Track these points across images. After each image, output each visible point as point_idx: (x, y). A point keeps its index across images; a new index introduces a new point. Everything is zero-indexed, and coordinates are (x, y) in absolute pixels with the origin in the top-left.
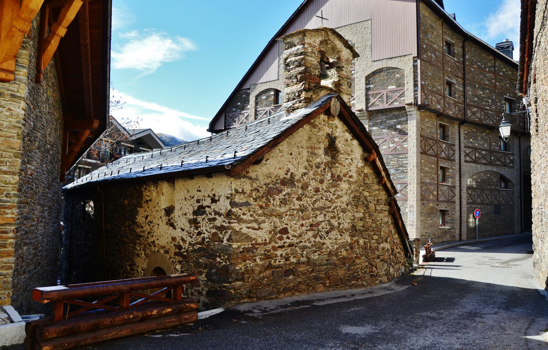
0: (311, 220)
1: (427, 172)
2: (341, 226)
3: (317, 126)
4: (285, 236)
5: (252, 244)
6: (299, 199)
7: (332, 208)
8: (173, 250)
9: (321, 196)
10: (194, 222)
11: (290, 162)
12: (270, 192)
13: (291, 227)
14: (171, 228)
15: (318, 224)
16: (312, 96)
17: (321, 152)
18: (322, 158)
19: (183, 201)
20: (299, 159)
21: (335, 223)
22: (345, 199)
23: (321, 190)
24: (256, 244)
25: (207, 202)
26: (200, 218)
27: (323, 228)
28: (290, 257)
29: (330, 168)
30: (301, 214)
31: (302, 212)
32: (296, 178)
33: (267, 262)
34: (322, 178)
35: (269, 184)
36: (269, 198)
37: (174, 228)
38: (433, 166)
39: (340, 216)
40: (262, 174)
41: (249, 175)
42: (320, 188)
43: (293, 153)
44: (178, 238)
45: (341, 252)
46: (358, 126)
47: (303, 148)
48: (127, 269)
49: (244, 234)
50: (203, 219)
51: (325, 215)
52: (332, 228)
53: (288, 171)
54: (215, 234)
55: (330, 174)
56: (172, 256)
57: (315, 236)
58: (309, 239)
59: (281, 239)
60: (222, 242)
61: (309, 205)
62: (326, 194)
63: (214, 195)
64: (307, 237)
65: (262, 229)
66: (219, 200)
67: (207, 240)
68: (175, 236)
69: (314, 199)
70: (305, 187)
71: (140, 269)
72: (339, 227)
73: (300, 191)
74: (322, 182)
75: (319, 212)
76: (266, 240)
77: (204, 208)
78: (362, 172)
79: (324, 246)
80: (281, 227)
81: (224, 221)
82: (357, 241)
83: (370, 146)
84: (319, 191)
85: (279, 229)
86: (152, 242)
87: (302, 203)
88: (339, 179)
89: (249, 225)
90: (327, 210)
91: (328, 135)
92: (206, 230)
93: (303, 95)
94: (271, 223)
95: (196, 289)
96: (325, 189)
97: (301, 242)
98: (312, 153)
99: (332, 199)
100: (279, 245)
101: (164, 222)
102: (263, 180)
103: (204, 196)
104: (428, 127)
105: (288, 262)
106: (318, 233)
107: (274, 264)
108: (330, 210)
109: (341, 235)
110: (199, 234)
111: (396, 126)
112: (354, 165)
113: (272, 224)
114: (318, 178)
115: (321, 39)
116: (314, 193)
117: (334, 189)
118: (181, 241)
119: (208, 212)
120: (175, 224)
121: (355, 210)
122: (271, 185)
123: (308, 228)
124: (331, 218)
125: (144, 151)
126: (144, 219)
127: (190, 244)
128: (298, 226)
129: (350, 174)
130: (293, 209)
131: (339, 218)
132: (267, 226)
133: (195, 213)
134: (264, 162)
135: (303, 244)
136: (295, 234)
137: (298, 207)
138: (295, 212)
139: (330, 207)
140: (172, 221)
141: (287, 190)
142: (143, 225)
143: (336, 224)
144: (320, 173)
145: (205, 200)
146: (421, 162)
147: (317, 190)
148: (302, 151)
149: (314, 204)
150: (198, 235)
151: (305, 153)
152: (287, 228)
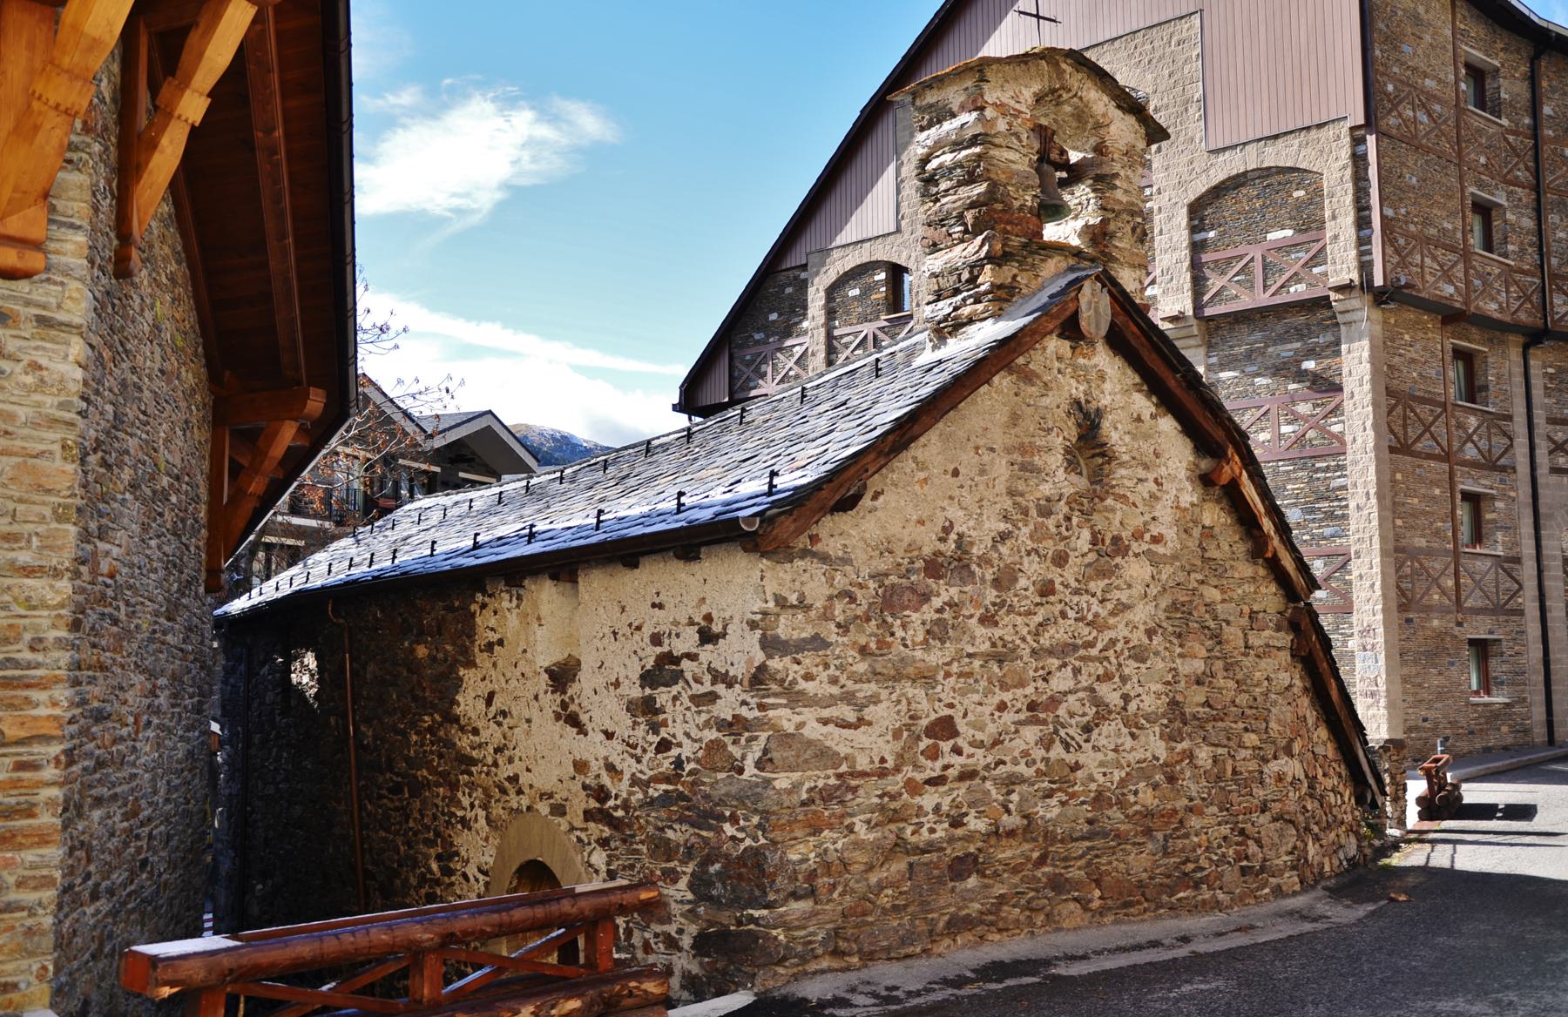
0: (1029, 690)
1: (1414, 514)
2: (1132, 707)
3: (1038, 377)
4: (946, 746)
5: (839, 776)
6: (988, 620)
7: (1100, 646)
8: (581, 803)
10: (646, 709)
11: (951, 498)
13: (965, 715)
15: (1054, 702)
16: (1015, 277)
17: (1056, 460)
18: (1059, 481)
19: (606, 640)
20: (981, 487)
22: (1142, 614)
23: (1058, 587)
25: (686, 641)
26: (663, 696)
27: (1072, 715)
30: (996, 668)
31: (1000, 662)
32: (975, 550)
34: (1061, 547)
35: (887, 575)
36: (890, 619)
38: (1437, 492)
40: (861, 544)
41: (819, 547)
42: (1058, 581)
47: (992, 450)
49: (810, 743)
50: (675, 698)
51: (1077, 671)
52: (1103, 712)
53: (947, 530)
55: (1086, 534)
56: (578, 823)
57: (1047, 743)
59: (933, 754)
61: (1024, 639)
62: (1076, 599)
64: (1018, 745)
65: (870, 724)
69: (1038, 619)
70: (1004, 580)
71: (471, 871)
72: (1124, 709)
73: (991, 595)
74: (1060, 560)
75: (1057, 663)
76: (883, 760)
77: (676, 660)
78: (1195, 522)
80: (933, 716)
81: (744, 703)
83: (1219, 434)
84: (1052, 592)
85: (924, 722)
87: (998, 632)
88: (1119, 547)
89: (826, 713)
90: (1082, 652)
93: (986, 278)
94: (899, 702)
95: (658, 928)
96: (1074, 584)
100: (928, 774)
102: (865, 564)
103: (676, 623)
104: (1413, 361)
105: (959, 832)
106: (1056, 732)
107: (913, 839)
108: (1094, 652)
109: (1133, 736)
112: (1167, 500)
113: (903, 706)
114: (1049, 547)
116: (1038, 600)
117: (1102, 584)
118: (604, 773)
119: (688, 675)
120: (584, 718)
122: (893, 579)
123: (1022, 716)
126: (481, 705)
127: (635, 781)
128: (987, 710)
129: (1155, 530)
130: (969, 655)
131: (1124, 679)
132: (884, 714)
136: (979, 736)
137: (986, 647)
138: (977, 663)
140: (572, 708)
141: (946, 592)
143: (1114, 699)
144: (1053, 530)
145: (678, 635)
146: (1394, 481)
147: (1046, 590)
148: (992, 462)
151: (1001, 468)
152: (951, 718)
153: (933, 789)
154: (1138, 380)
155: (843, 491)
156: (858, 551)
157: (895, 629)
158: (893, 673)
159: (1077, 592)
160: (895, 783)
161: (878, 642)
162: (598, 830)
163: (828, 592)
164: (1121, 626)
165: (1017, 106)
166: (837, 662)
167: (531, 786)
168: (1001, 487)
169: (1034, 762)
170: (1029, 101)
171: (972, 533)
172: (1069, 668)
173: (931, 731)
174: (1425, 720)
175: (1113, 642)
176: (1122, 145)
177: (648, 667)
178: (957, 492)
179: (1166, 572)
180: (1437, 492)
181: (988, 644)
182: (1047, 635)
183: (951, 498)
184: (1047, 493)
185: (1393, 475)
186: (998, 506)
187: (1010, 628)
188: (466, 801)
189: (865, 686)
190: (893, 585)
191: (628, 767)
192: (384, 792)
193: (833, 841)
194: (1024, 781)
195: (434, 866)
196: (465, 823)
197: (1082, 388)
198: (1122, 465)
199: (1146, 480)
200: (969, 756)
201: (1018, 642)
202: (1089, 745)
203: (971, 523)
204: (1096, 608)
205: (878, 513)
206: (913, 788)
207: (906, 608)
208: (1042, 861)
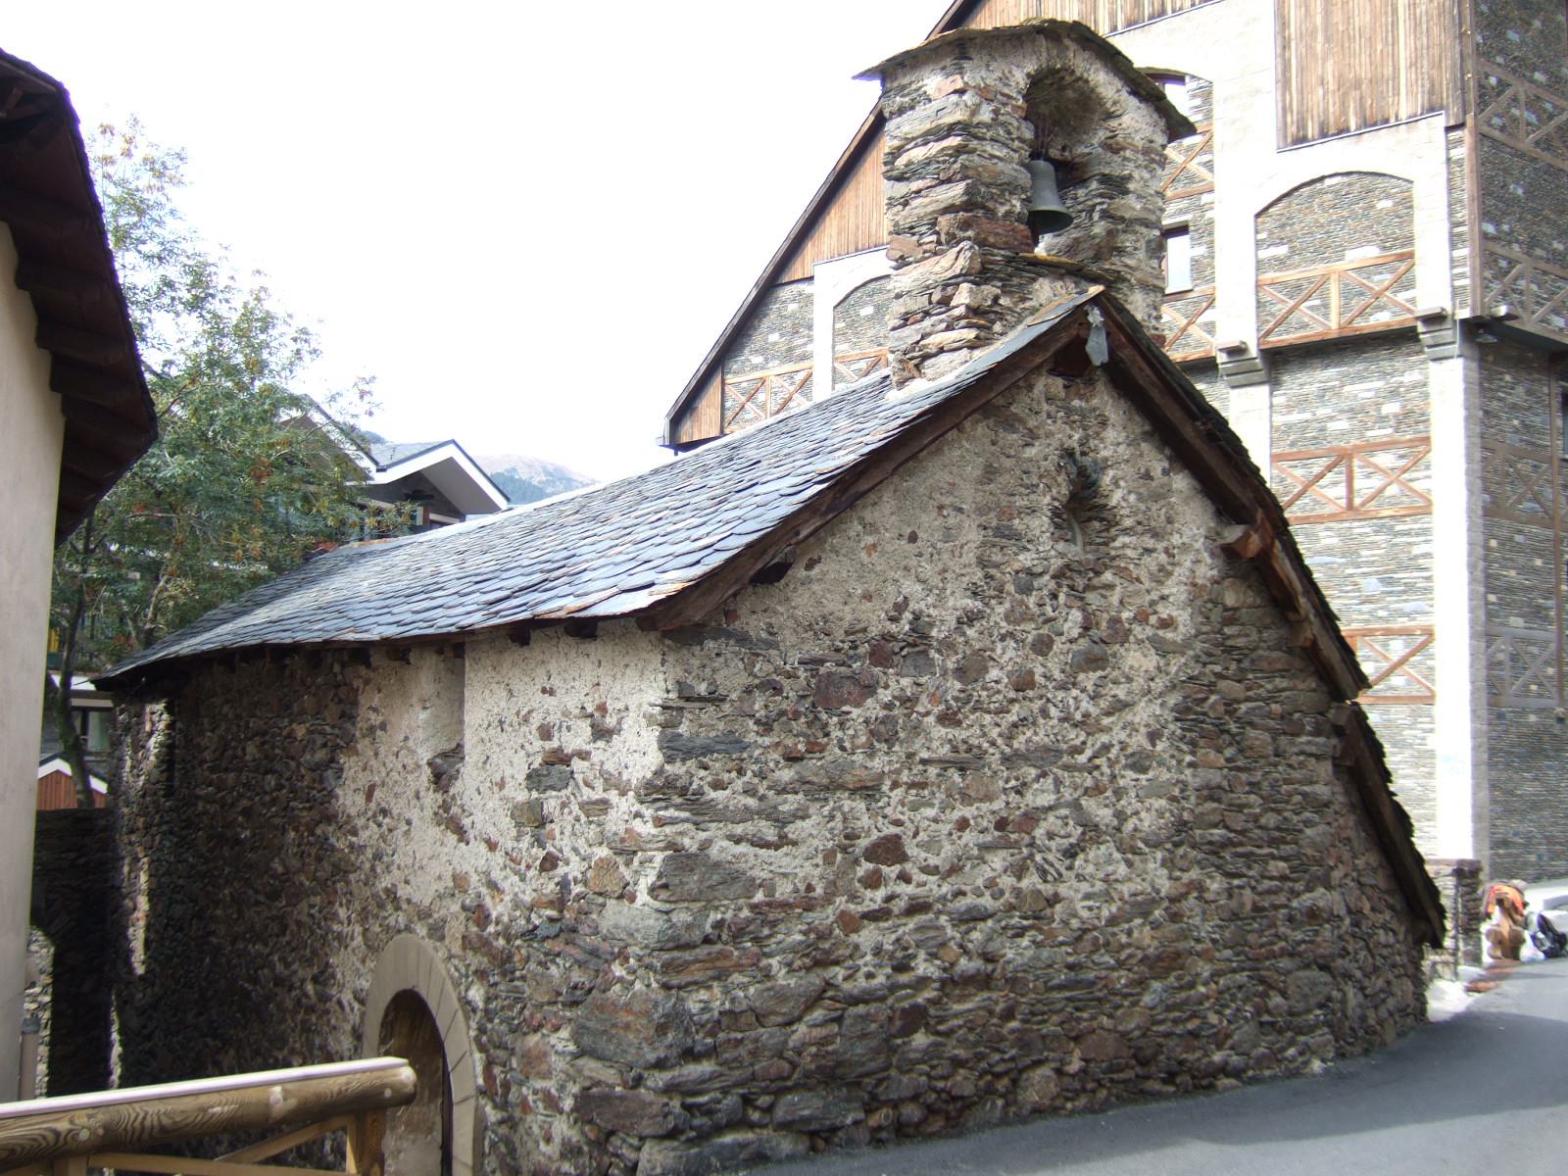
0: (998, 804)
1: (1510, 589)
2: (1129, 826)
3: (1021, 421)
4: (891, 871)
5: (753, 907)
6: (948, 719)
7: (1088, 753)
8: (456, 928)
9: (1040, 703)
10: (534, 820)
11: (906, 568)
12: (828, 693)
13: (916, 834)
14: (452, 838)
15: (1031, 818)
16: (996, 299)
17: (1040, 525)
18: (1043, 546)
19: (492, 731)
20: (945, 556)
21: (1101, 813)
22: (1144, 713)
23: (1038, 679)
24: (769, 904)
25: (577, 737)
26: (551, 803)
27: (1051, 836)
28: (915, 957)
29: (1078, 596)
30: (957, 778)
31: (962, 769)
32: (934, 633)
33: (815, 979)
34: (1045, 630)
35: (822, 662)
36: (824, 717)
37: (461, 833)
38: (1538, 562)
39: (1122, 782)
40: (790, 623)
41: (737, 625)
42: (1039, 670)
43: (921, 535)
44: (474, 878)
45: (1129, 933)
46: (1193, 417)
47: (960, 510)
48: (306, 995)
49: (717, 865)
50: (564, 805)
51: (1058, 782)
52: (1092, 832)
53: (900, 608)
54: (605, 866)
55: (1076, 616)
56: (456, 949)
57: (1019, 871)
58: (991, 884)
59: (873, 881)
60: (632, 899)
61: (993, 744)
62: (1060, 695)
63: (602, 708)
64: (981, 876)
65: (794, 843)
66: (617, 730)
67: (577, 889)
68: (466, 868)
69: (1013, 718)
70: (970, 671)
71: (347, 997)
72: (1118, 830)
73: (955, 686)
74: (1042, 646)
75: (1033, 772)
76: (810, 888)
77: (566, 760)
78: (1215, 603)
79: (1058, 907)
80: (875, 835)
81: (638, 815)
82: (1200, 887)
83: (1245, 497)
84: (1031, 685)
85: (863, 843)
86: (387, 891)
87: (960, 734)
88: (1119, 633)
89: (739, 829)
90: (1066, 759)
91: (1069, 453)
92: (575, 850)
93: (963, 296)
94: (832, 818)
95: (540, 1084)
96: (1057, 675)
97: (962, 893)
98: (999, 532)
99: (1086, 715)
100: (868, 906)
101: (428, 813)
102: (795, 648)
103: (566, 714)
104: (1514, 407)
105: (904, 978)
106: (1031, 856)
107: (847, 986)
108: (1082, 759)
109: (1129, 864)
110: (549, 863)
111: (1378, 405)
112: (1181, 573)
113: (838, 824)
114: (1030, 631)
115: (1031, 67)
116: (1012, 694)
117: (1094, 676)
118: (484, 890)
119: (579, 777)
120: (466, 822)
121: (1188, 758)
122: (829, 666)
123: (988, 838)
124: (1086, 792)
125: (442, 524)
126: (360, 799)
127: (517, 904)
128: (945, 828)
129: (1164, 611)
130: (924, 762)
131: (1119, 793)
132: (813, 830)
133: (534, 779)
134: (799, 572)
135: (968, 901)
136: (933, 861)
137: (944, 751)
138: (933, 771)
139: (1077, 750)
140: (454, 810)
141: (896, 683)
142: (360, 822)
143: (1103, 815)
144: (1035, 610)
145: (569, 729)
146: (1487, 548)
147: (1023, 683)
148: (960, 527)
149: (1009, 738)
150: (543, 869)
151: (972, 536)
152: (898, 837)
153: (873, 926)
154: (1147, 428)
155: (767, 558)
156: (787, 632)
157: (831, 728)
158: (825, 781)
159: (1063, 687)
160: (825, 916)
161: (809, 743)
162: (477, 961)
163: (744, 680)
164: (1116, 729)
165: (1006, 91)
166: (755, 768)
167: (409, 901)
168: (970, 557)
169: (1002, 893)
170: (1022, 85)
171: (932, 611)
172: (1050, 780)
173: (871, 854)
174: (1516, 834)
175: (1107, 748)
176: (1138, 140)
177: (536, 765)
178: (913, 562)
179: (1175, 664)
180: (1538, 562)
181: (947, 747)
182: (1022, 738)
183: (906, 568)
184: (1029, 564)
185: (1486, 541)
186: (966, 579)
187: (980, 730)
188: (342, 913)
189: (790, 797)
190: (830, 674)
191: (510, 883)
192: (261, 898)
193: (747, 991)
194: (991, 916)
195: (310, 988)
196: (339, 937)
197: (1076, 437)
198: (1126, 531)
199: (1153, 550)
200: (919, 885)
201: (986, 745)
202: (1072, 874)
203: (930, 600)
204: (1086, 705)
205: (815, 587)
206: (849, 923)
207: (845, 703)
208: (1009, 1014)
